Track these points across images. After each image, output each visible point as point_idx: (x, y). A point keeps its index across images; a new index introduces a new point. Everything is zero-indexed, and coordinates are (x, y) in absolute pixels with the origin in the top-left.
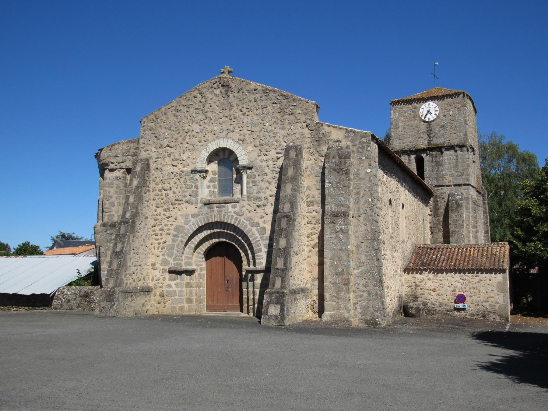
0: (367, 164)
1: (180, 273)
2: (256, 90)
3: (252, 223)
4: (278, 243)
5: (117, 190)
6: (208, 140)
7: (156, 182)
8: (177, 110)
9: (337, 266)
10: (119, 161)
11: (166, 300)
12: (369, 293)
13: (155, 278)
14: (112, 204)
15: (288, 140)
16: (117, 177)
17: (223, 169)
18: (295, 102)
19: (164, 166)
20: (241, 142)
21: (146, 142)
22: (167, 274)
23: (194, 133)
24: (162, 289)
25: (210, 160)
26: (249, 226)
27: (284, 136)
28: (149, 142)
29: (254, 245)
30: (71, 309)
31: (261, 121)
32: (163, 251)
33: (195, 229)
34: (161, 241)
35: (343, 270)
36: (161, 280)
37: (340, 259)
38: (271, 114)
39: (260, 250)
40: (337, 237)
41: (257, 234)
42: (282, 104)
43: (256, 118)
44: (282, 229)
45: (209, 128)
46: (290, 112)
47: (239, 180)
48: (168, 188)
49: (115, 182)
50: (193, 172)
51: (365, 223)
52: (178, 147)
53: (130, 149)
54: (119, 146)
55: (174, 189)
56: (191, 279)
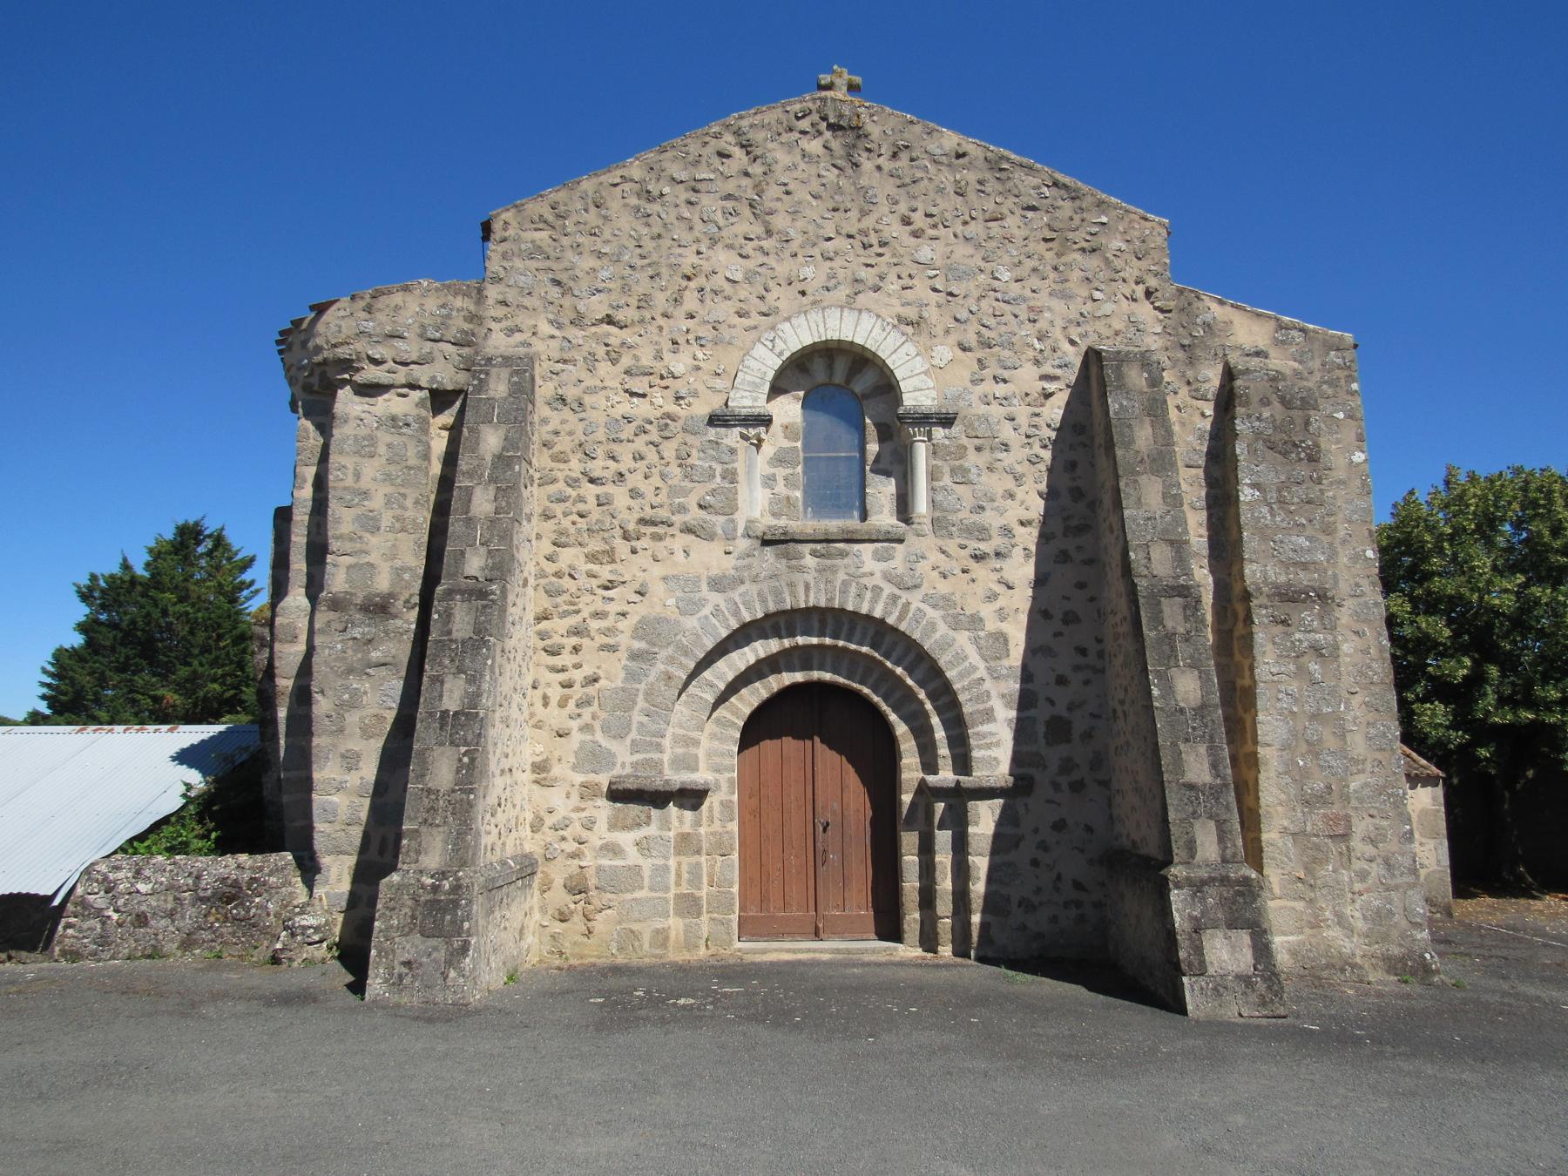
0: (1353, 436)
1: (657, 798)
2: (964, 155)
3: (955, 616)
4: (1169, 690)
5: (392, 468)
6: (776, 310)
7: (556, 449)
8: (648, 196)
9: (1305, 774)
10: (405, 357)
11: (597, 903)
12: (1387, 863)
13: (550, 820)
14: (370, 523)
15: (1081, 336)
16: (394, 419)
17: (823, 420)
18: (1103, 212)
19: (590, 391)
20: (909, 330)
21: (511, 296)
22: (603, 802)
23: (718, 281)
24: (576, 862)
25: (777, 389)
26: (942, 629)
27: (1070, 321)
28: (527, 301)
29: (962, 698)
30: (155, 953)
31: (983, 264)
32: (586, 712)
33: (724, 633)
34: (578, 676)
35: (1329, 787)
36: (576, 829)
37: (1314, 749)
38: (1019, 242)
39: (988, 716)
40: (1302, 672)
41: (974, 658)
42: (1058, 214)
43: (962, 251)
44: (1170, 636)
45: (783, 268)
46: (1085, 245)
47: (898, 464)
48: (608, 474)
49: (384, 437)
50: (715, 420)
51: (1357, 627)
52: (653, 329)
53: (449, 316)
54: (409, 298)
55: (634, 480)
56: (698, 823)
